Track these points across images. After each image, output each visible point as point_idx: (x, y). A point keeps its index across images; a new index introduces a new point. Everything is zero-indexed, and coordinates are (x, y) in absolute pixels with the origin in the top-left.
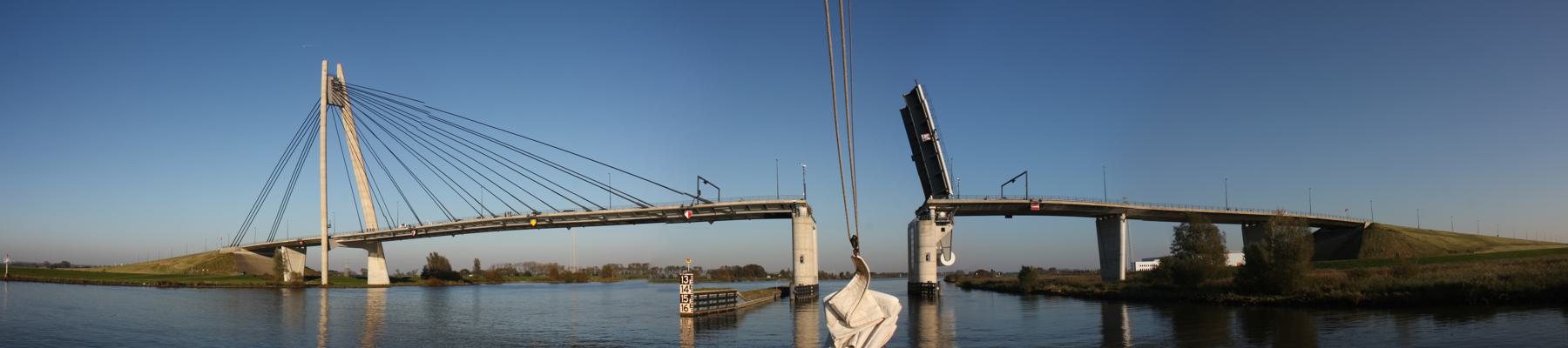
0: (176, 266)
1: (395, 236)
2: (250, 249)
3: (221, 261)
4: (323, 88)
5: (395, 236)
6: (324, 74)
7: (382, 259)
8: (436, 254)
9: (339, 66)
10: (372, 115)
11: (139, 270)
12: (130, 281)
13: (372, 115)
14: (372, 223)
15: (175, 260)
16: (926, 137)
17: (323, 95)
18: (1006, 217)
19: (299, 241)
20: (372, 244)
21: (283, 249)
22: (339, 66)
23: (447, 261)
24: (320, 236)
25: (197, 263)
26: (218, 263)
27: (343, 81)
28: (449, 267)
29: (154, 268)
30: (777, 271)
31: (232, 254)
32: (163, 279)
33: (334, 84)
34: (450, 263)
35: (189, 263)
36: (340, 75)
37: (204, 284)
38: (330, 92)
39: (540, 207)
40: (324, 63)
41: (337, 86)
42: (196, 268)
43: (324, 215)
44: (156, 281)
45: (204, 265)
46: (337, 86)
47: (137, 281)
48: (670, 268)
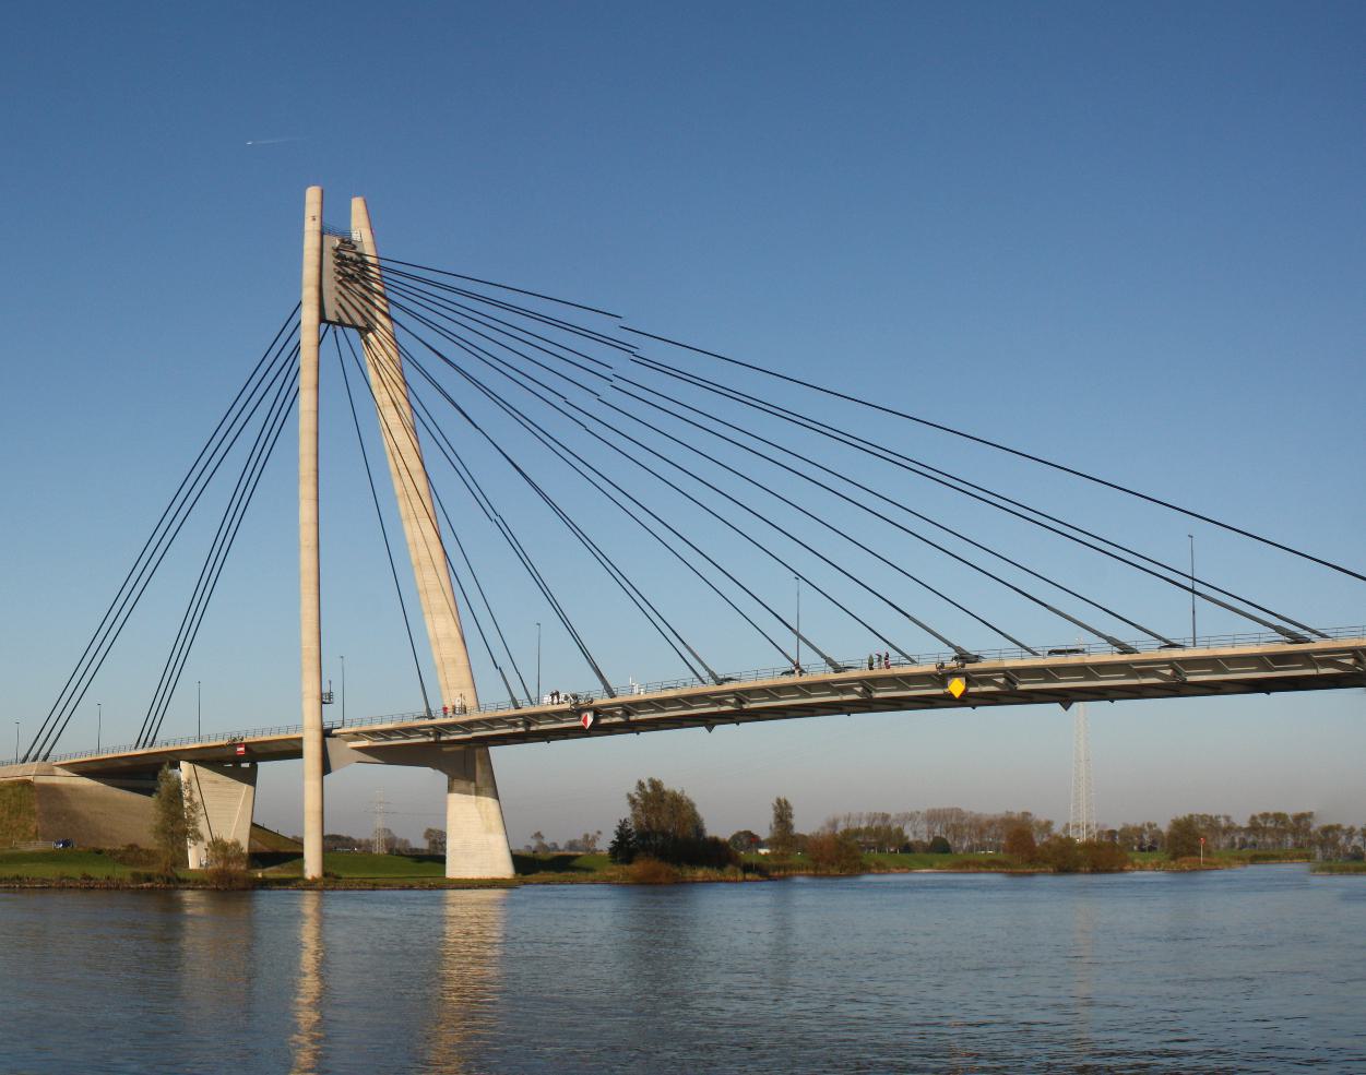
1: (529, 730)
5: (529, 730)
6: (311, 228)
8: (655, 785)
9: (357, 205)
21: (185, 770)
22: (357, 205)
24: (298, 727)
33: (342, 261)
36: (360, 231)
38: (330, 284)
40: (312, 195)
41: (350, 267)
46: (350, 267)
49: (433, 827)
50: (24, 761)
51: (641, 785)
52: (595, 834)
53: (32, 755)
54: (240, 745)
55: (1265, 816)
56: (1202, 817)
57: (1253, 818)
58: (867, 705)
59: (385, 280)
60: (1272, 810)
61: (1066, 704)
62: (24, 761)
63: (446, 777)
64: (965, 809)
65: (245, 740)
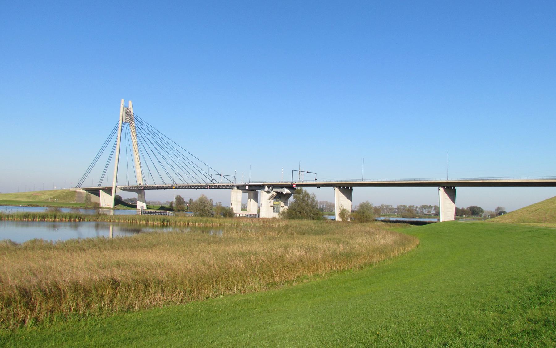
0: (43, 197)
1: (148, 188)
2: (86, 190)
3: (68, 195)
4: (121, 114)
5: (148, 188)
6: (122, 106)
7: (257, 203)
8: (180, 196)
9: (130, 102)
10: (155, 144)
11: (17, 197)
12: (14, 204)
13: (155, 144)
14: (140, 182)
15: (43, 193)
16: (247, 187)
17: (121, 117)
18: (318, 188)
19: (106, 188)
20: (139, 190)
21: (101, 191)
22: (130, 102)
23: (118, 196)
24: (112, 186)
25: (55, 195)
26: (66, 196)
27: (132, 111)
28: (121, 199)
29: (28, 197)
30: (494, 210)
31: (75, 192)
32: (31, 204)
33: (127, 112)
34: (119, 195)
35: (51, 195)
36: (131, 107)
37: (49, 206)
38: (124, 116)
39: (201, 182)
40: (123, 100)
41: (128, 113)
42: (53, 198)
43: (115, 177)
44: (26, 204)
45: (58, 197)
46: (128, 113)
47: (17, 204)
48: (424, 207)
49: (383, 204)
50: (76, 187)
51: (177, 196)
52: (245, 204)
53: (78, 186)
54: (294, 184)
55: (401, 206)
56: (385, 205)
57: (398, 206)
58: (157, 189)
59: (134, 117)
60: (403, 204)
61: (319, 188)
62: (76, 187)
63: (138, 194)
64: (328, 201)
65: (296, 183)
